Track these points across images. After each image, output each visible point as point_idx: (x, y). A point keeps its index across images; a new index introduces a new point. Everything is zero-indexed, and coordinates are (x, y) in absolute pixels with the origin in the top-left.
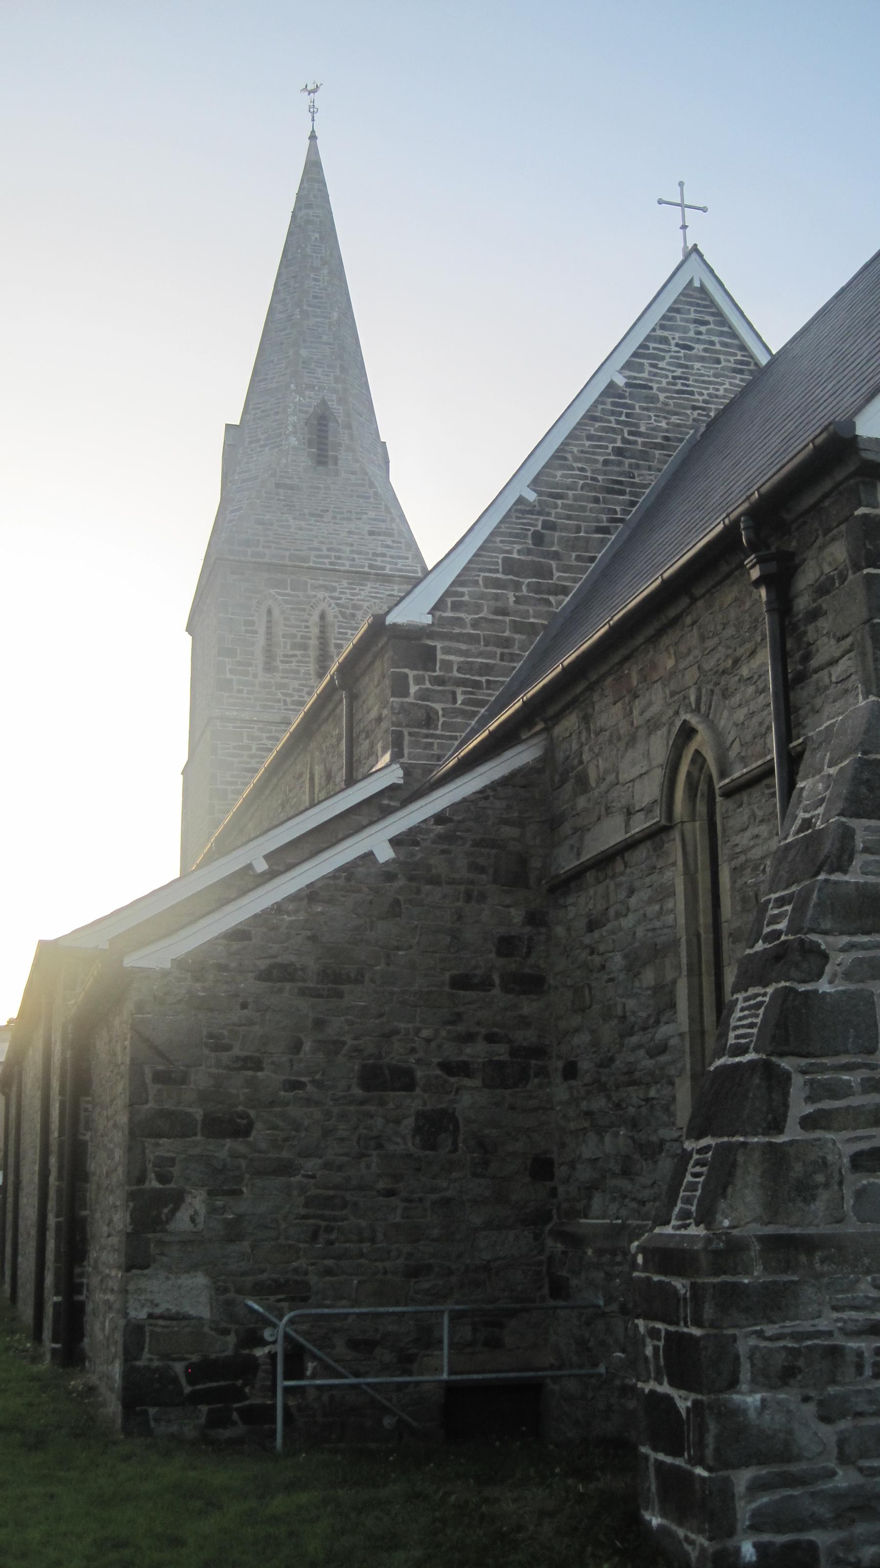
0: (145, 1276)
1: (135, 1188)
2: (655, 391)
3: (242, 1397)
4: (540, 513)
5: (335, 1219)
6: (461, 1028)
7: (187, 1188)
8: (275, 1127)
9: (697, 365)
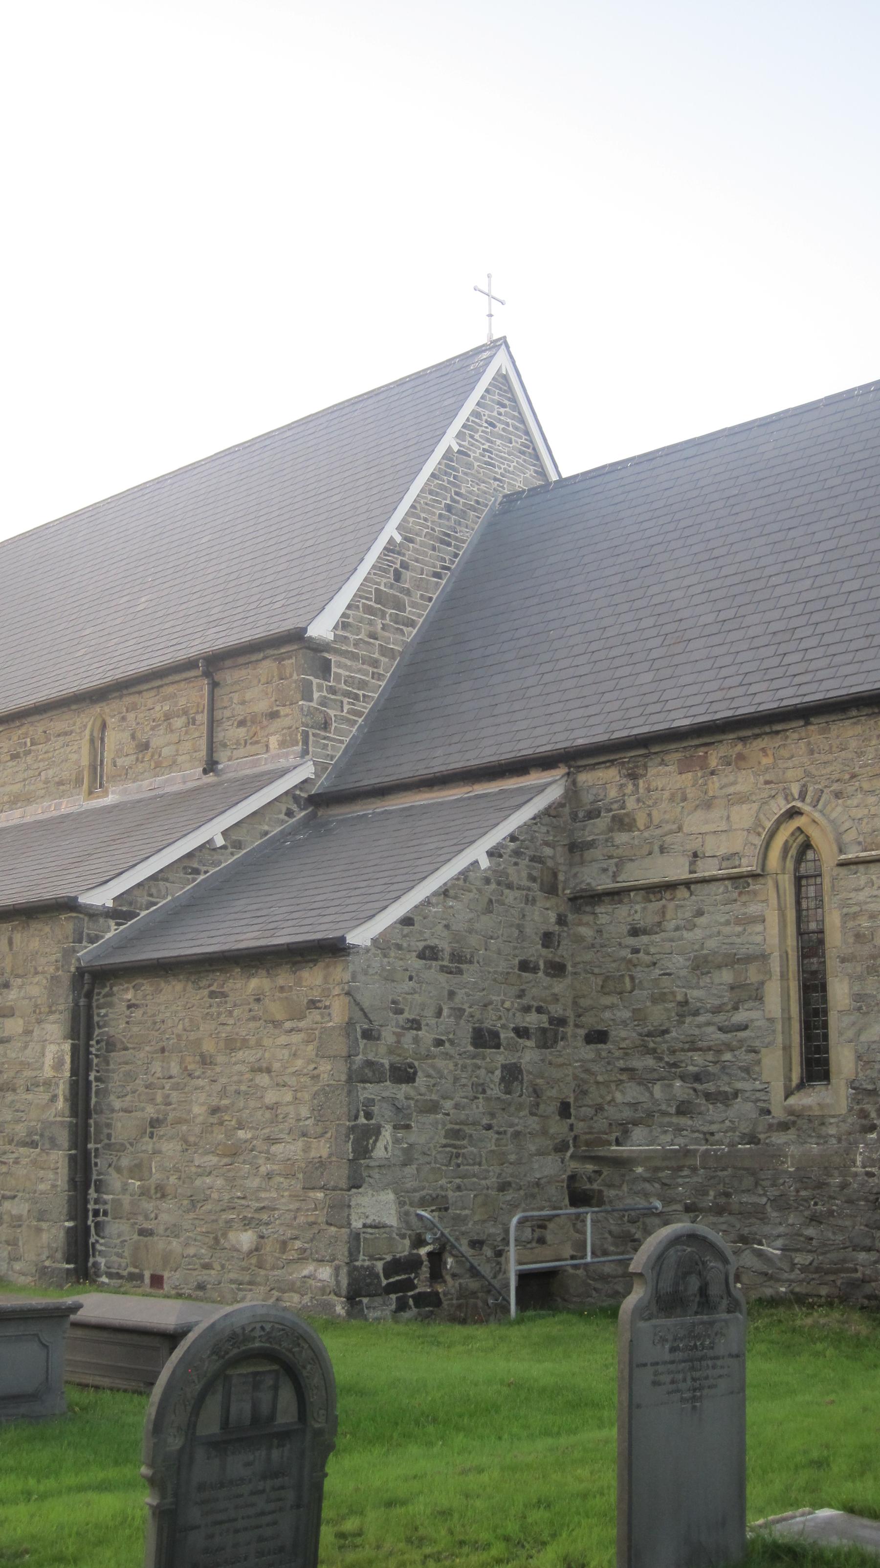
0: (360, 1193)
1: (353, 1123)
2: (471, 459)
3: (414, 1287)
4: (399, 553)
5: (460, 1147)
6: (525, 1001)
7: (382, 1123)
8: (429, 1076)
9: (498, 442)
